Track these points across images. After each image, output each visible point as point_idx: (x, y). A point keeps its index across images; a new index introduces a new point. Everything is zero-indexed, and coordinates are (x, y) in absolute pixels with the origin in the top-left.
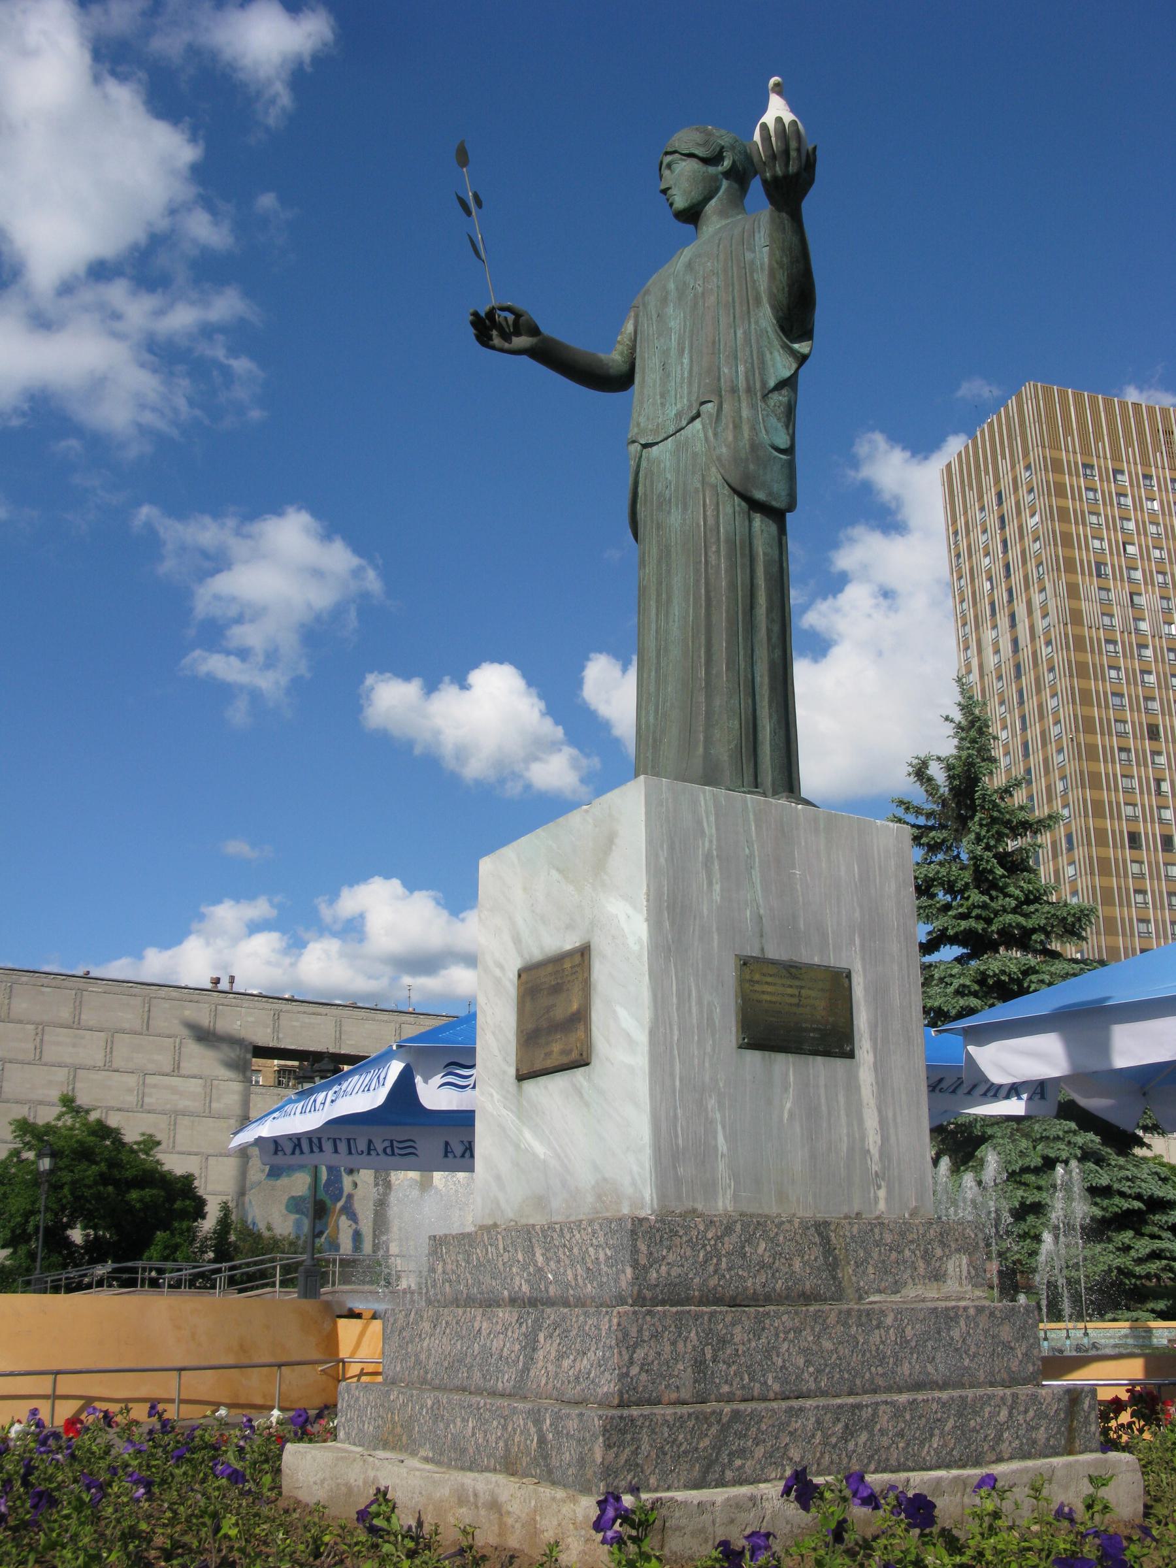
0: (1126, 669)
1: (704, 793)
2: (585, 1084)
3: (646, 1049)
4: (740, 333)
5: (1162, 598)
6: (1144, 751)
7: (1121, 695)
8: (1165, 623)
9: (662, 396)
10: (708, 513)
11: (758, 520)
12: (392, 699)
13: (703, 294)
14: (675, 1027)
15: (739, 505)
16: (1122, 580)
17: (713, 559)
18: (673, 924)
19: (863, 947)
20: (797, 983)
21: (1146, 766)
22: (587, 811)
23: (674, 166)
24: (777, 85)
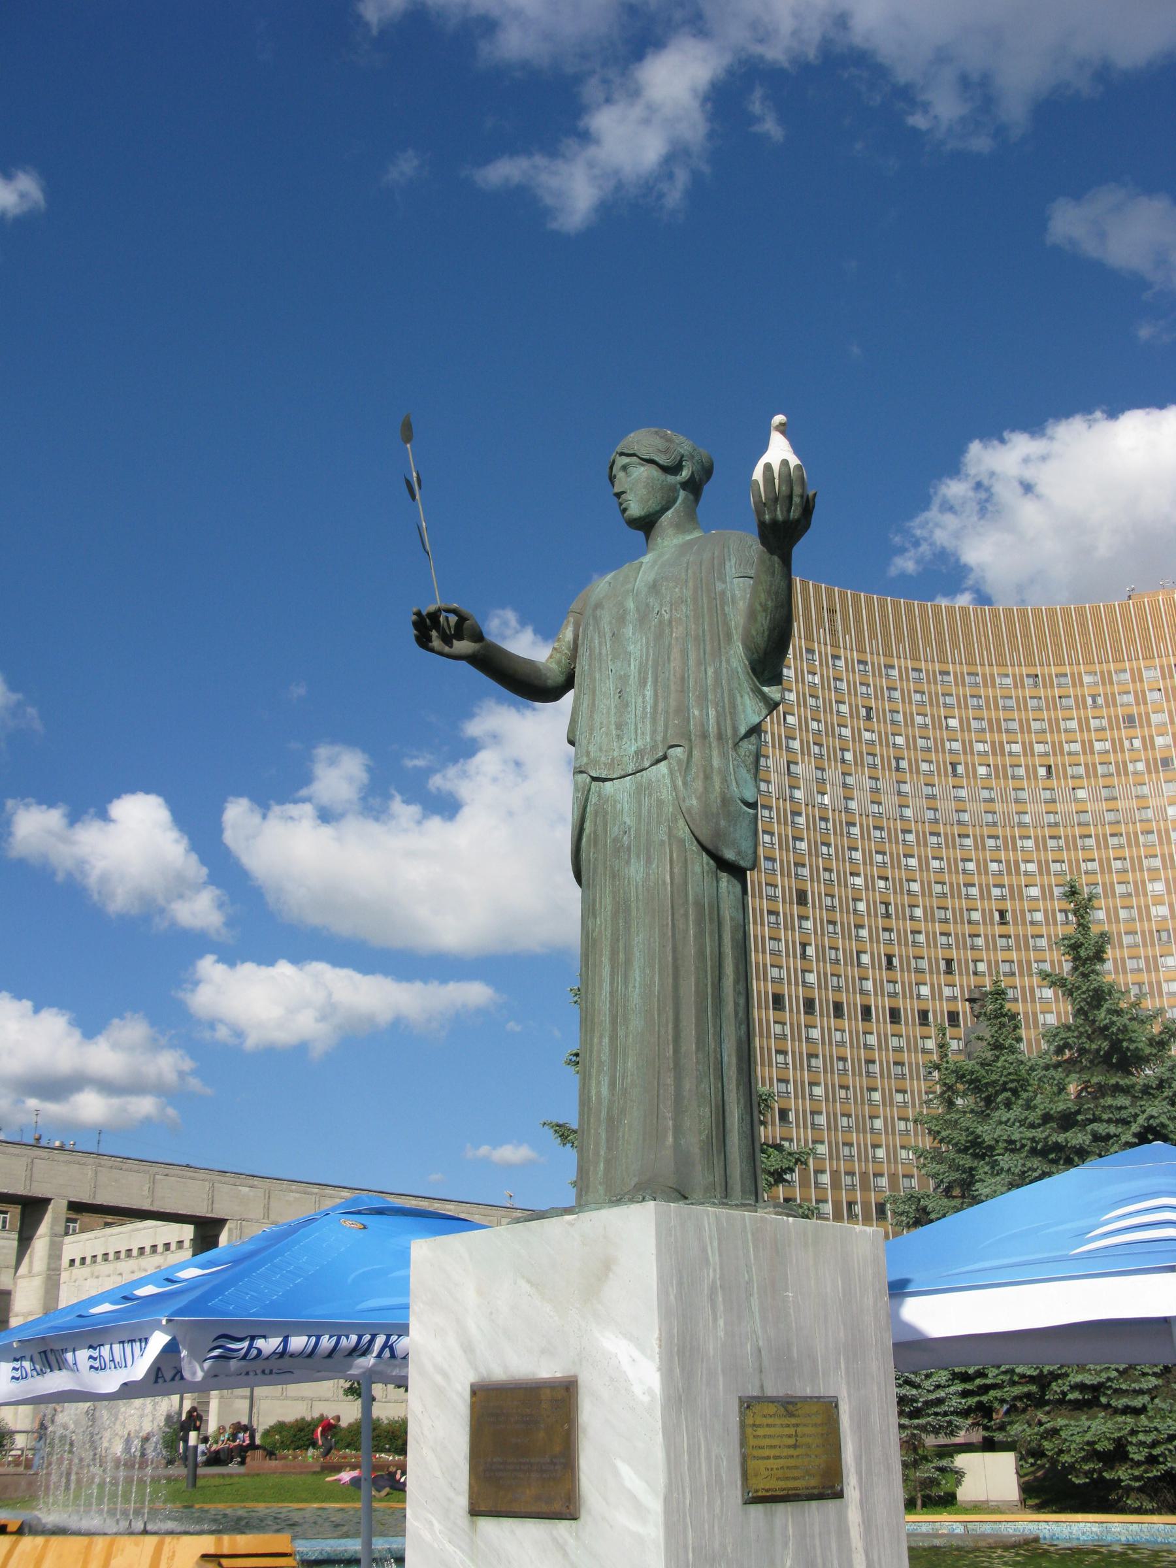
0: (780, 835)
1: (708, 1215)
2: (571, 1541)
3: (660, 1519)
4: (710, 671)
5: (817, 768)
6: (792, 916)
7: (773, 860)
8: (818, 792)
9: (619, 726)
10: (676, 870)
11: (724, 877)
12: (35, 826)
13: (670, 622)
14: (687, 1490)
15: (708, 864)
16: (781, 748)
17: (680, 924)
18: (683, 1370)
19: (847, 1368)
20: (793, 1421)
21: (793, 929)
22: (571, 1224)
23: (630, 469)
24: (781, 424)
